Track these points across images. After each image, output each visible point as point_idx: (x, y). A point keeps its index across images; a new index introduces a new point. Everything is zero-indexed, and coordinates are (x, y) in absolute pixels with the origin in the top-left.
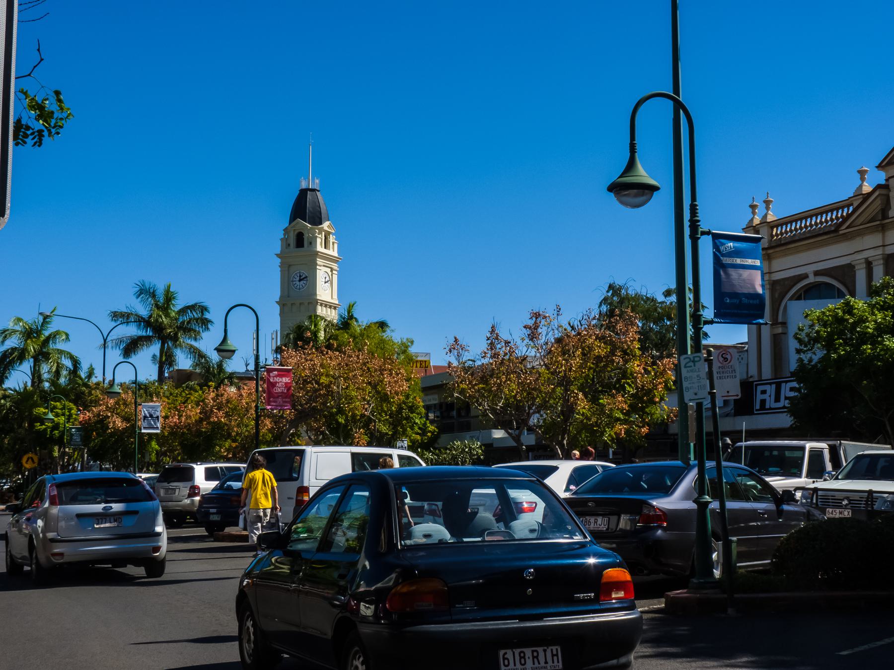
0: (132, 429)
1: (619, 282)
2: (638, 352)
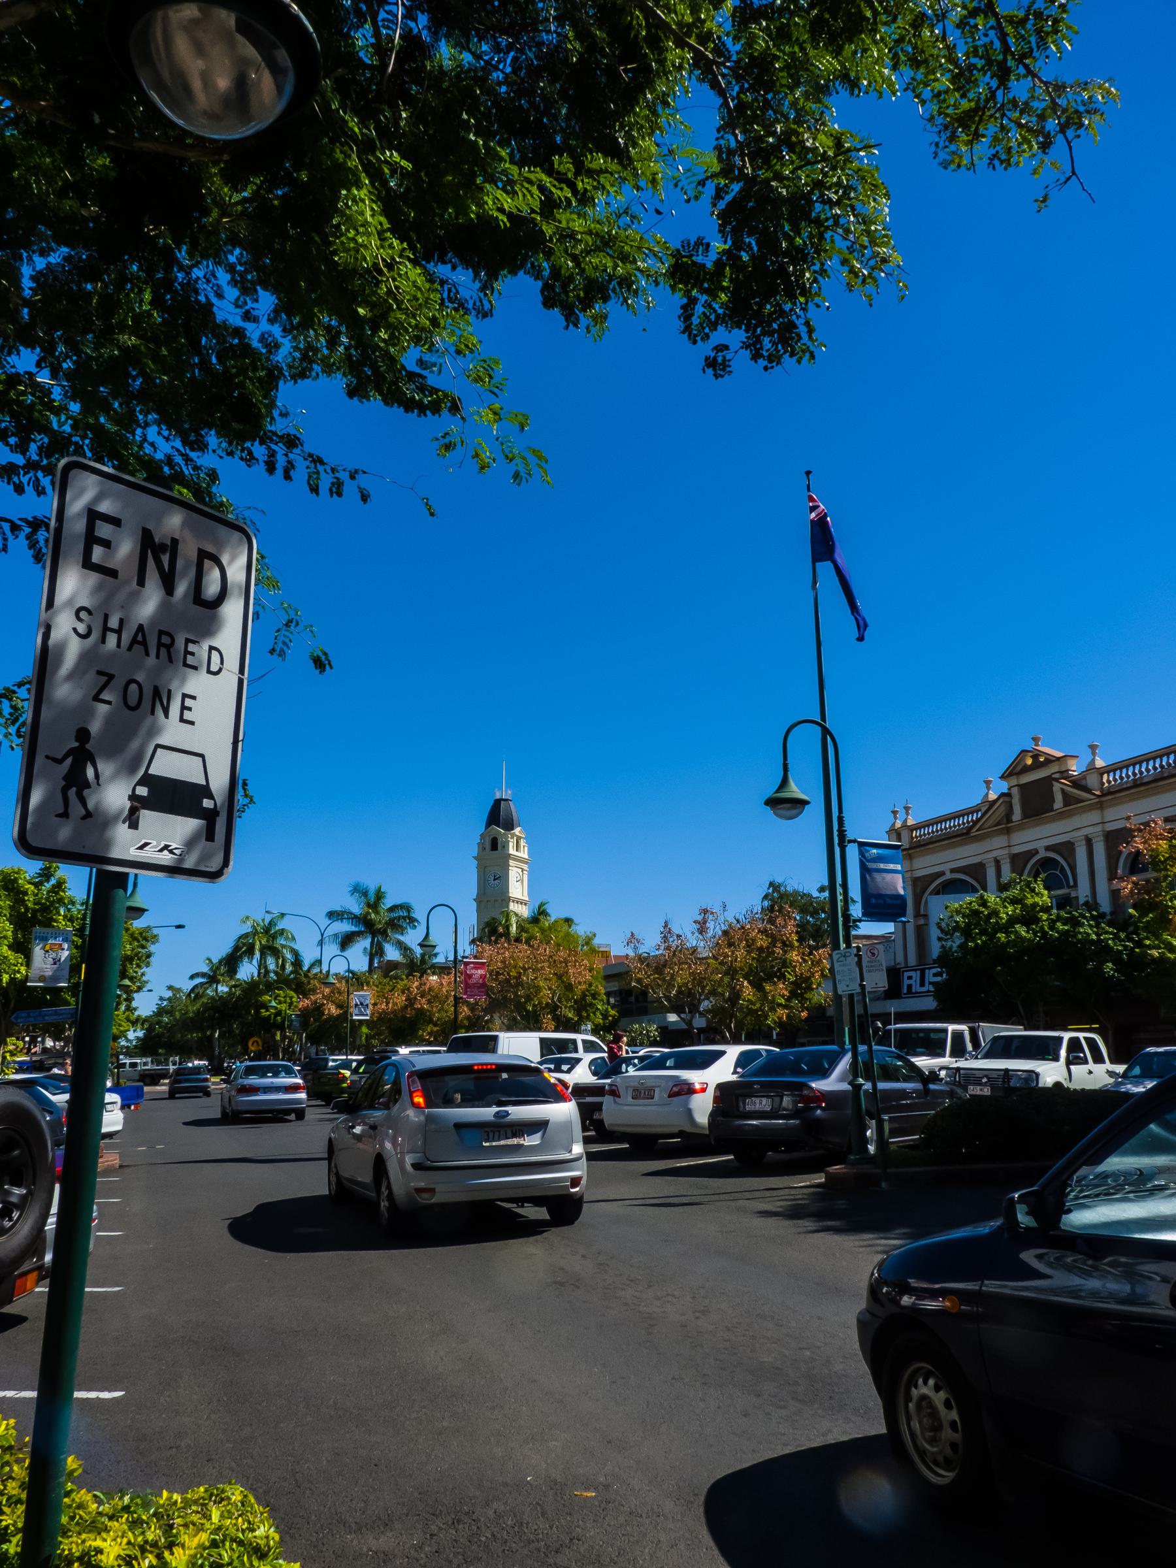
0: (345, 1016)
1: (778, 880)
2: (796, 944)
